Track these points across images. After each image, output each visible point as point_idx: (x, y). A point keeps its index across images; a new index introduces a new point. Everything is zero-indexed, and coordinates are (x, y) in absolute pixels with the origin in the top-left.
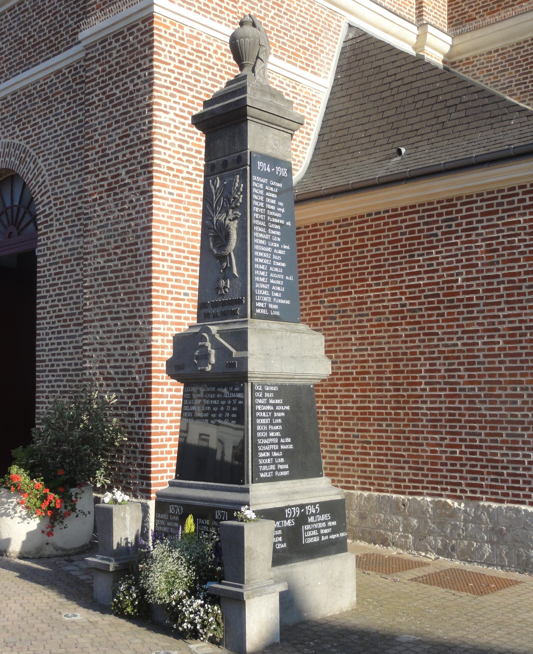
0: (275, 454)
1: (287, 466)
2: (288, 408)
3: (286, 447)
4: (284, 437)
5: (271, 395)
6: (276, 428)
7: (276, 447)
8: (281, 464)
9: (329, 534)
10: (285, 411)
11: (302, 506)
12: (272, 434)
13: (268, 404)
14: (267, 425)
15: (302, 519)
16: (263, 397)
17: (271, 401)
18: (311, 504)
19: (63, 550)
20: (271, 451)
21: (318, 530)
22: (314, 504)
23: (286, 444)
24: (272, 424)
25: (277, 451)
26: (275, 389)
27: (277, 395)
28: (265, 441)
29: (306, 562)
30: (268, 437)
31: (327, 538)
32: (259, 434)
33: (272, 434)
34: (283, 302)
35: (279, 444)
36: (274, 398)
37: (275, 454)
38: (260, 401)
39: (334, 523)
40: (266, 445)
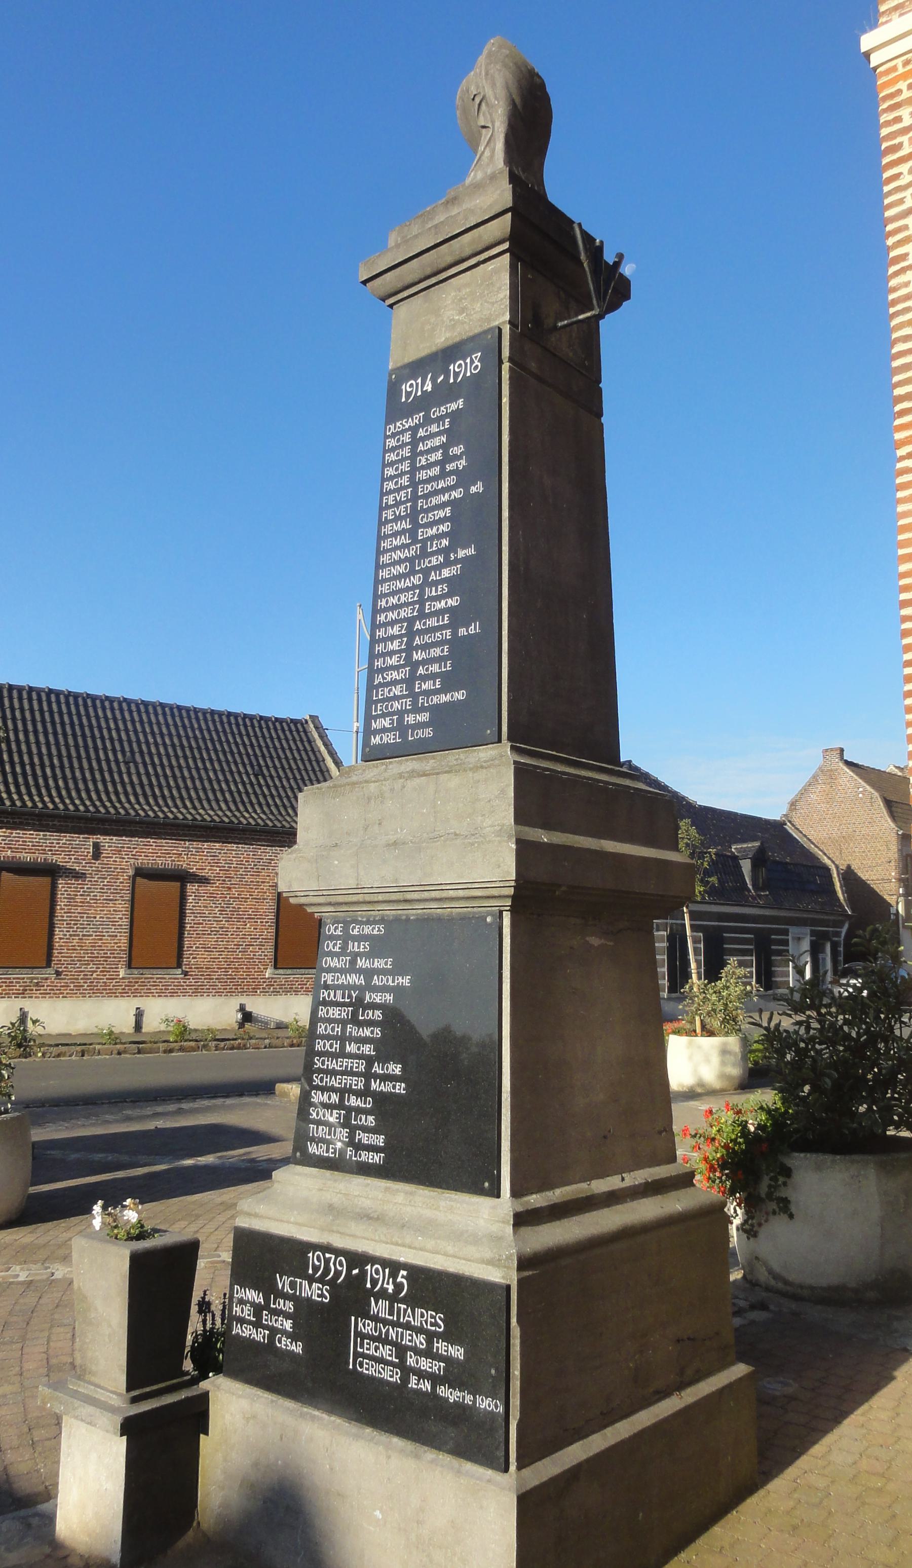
0: (354, 1101)
1: (380, 1140)
2: (405, 981)
3: (387, 1087)
4: (383, 1057)
5: (364, 947)
6: (367, 1032)
7: (358, 1084)
8: (365, 1129)
9: (435, 1380)
10: (397, 991)
11: (357, 1260)
12: (351, 1048)
13: (352, 969)
14: (343, 1023)
15: (352, 1295)
16: (344, 951)
17: (361, 963)
18: (385, 1263)
19: (786, 1282)
20: (343, 1092)
21: (401, 1351)
22: (394, 1267)
23: (385, 1078)
24: (355, 1021)
25: (359, 1094)
26: (376, 930)
27: (378, 947)
28: (332, 1065)
29: (352, 1428)
30: (342, 1054)
31: (426, 1386)
32: (319, 1046)
33: (351, 1048)
34: (444, 698)
35: (368, 1075)
36: (369, 955)
37: (354, 1101)
38: (334, 963)
39: (457, 1352)
40: (333, 1073)
